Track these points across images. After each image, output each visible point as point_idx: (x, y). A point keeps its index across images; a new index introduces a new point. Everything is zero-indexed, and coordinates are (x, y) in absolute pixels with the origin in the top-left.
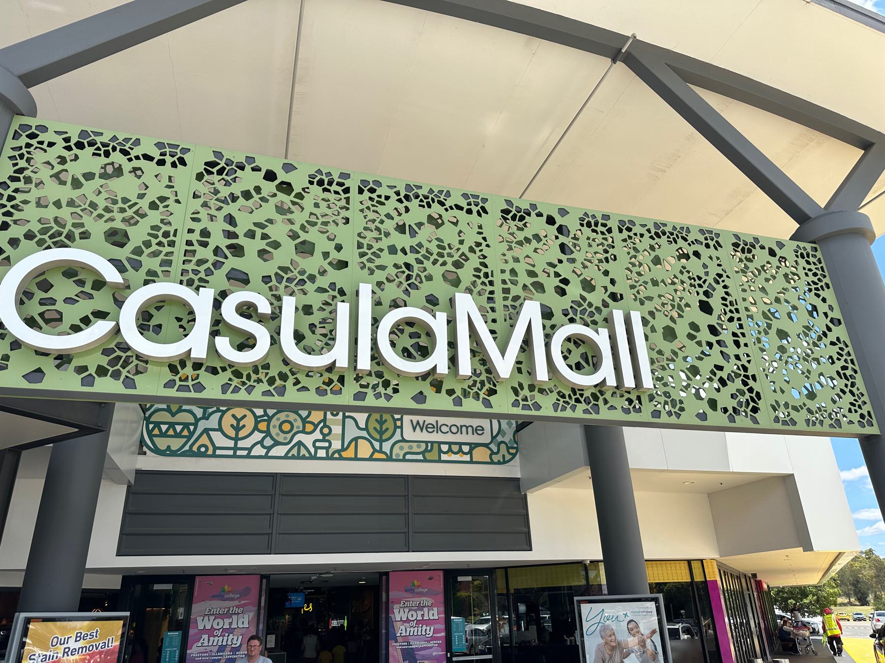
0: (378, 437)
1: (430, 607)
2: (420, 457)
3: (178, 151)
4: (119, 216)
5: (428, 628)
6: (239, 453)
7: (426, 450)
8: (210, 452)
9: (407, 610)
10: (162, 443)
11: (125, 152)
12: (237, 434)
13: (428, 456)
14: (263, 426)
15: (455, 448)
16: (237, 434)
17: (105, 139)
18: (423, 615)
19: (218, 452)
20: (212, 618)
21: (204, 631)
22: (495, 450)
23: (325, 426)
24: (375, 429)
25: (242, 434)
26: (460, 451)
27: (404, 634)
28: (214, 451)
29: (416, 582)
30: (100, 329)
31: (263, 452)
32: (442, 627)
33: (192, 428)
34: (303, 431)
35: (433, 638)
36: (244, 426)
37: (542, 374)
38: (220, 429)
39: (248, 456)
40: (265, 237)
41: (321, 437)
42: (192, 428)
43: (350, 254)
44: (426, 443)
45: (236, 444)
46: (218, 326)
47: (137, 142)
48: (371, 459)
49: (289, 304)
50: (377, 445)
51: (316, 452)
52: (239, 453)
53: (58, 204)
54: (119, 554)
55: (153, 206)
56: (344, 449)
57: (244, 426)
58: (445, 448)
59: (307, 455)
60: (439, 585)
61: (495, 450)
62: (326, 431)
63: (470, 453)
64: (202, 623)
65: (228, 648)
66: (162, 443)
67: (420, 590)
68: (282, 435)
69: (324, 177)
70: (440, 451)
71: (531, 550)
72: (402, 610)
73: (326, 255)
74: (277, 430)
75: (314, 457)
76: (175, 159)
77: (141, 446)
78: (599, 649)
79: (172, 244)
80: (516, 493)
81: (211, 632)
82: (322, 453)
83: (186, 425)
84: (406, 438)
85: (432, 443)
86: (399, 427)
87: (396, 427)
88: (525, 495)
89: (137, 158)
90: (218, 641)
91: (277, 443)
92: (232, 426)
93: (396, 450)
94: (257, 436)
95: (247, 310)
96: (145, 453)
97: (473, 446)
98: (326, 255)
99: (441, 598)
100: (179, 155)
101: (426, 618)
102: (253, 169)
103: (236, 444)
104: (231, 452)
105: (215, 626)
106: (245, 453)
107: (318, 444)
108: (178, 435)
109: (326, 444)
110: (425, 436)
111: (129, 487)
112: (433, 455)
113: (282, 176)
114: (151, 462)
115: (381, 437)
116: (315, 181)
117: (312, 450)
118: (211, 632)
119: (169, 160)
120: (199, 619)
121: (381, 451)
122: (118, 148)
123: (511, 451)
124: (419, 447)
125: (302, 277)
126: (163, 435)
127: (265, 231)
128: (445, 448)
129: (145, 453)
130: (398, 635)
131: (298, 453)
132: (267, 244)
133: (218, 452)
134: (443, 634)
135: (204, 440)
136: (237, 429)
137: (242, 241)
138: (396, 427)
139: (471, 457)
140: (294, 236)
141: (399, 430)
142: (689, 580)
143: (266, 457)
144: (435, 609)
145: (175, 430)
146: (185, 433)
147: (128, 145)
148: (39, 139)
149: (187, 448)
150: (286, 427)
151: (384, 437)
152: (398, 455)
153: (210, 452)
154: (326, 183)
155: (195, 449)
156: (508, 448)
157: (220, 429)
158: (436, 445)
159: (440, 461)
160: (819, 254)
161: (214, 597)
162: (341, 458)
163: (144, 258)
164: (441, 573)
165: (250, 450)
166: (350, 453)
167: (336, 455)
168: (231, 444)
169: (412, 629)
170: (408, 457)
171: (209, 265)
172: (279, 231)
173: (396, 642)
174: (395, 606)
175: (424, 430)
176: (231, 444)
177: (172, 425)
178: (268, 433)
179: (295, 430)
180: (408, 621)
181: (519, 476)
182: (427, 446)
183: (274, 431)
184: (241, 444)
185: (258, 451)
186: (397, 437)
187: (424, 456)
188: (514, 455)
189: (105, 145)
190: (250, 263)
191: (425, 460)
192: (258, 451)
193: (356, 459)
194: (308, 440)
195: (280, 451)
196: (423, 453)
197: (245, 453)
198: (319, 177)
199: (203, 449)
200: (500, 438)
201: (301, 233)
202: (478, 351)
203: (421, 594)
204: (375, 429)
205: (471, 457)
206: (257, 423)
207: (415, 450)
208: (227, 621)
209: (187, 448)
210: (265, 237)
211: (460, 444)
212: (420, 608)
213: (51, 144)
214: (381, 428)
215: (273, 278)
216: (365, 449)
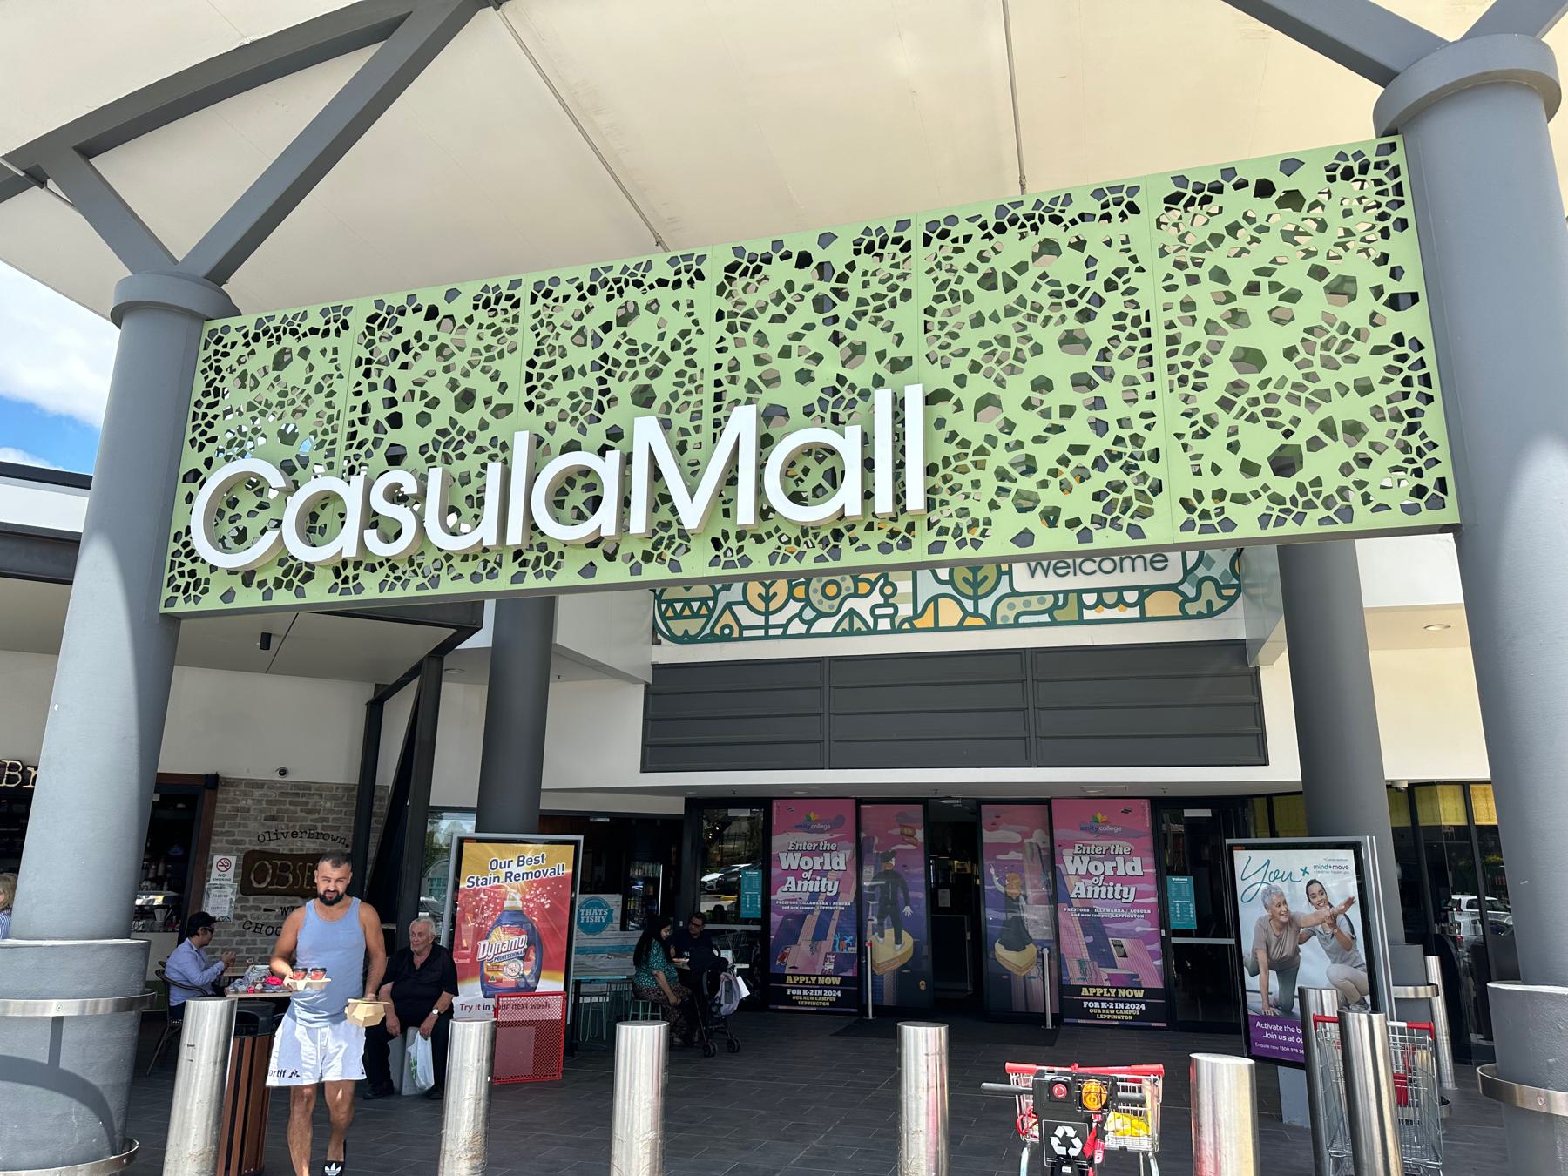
0: (970, 591)
1: (1128, 857)
2: (1045, 618)
3: (1124, 194)
4: (1071, 313)
5: (1126, 889)
6: (772, 632)
7: (1055, 606)
8: (736, 634)
9: (1086, 859)
10: (678, 627)
11: (1056, 220)
12: (767, 607)
13: (1059, 615)
14: (799, 592)
15: (1110, 598)
16: (767, 607)
17: (1027, 209)
18: (822, 864)
19: (746, 633)
20: (798, 855)
21: (790, 871)
22: (1191, 593)
23: (887, 583)
24: (965, 579)
25: (773, 605)
26: (1121, 601)
27: (1083, 895)
28: (741, 633)
29: (1099, 816)
30: (272, 536)
31: (802, 628)
32: (1152, 888)
33: (711, 603)
34: (856, 595)
35: (1134, 905)
36: (775, 594)
37: (745, 513)
38: (745, 602)
39: (784, 636)
40: (1275, 287)
41: (882, 601)
42: (711, 603)
43: (517, 395)
44: (1055, 593)
45: (767, 620)
46: (371, 519)
47: (1068, 199)
48: (960, 627)
49: (435, 477)
50: (969, 605)
51: (876, 624)
52: (772, 632)
53: (995, 318)
54: (643, 770)
55: (1110, 286)
56: (917, 616)
57: (775, 594)
58: (1090, 599)
59: (864, 629)
60: (1143, 819)
61: (1191, 593)
62: (888, 590)
63: (1140, 603)
64: (787, 862)
65: (822, 897)
66: (678, 627)
67: (1109, 828)
68: (827, 603)
69: (1351, 163)
70: (1082, 606)
71: (1266, 763)
72: (1077, 858)
73: (1378, 291)
74: (819, 596)
75: (873, 631)
76: (1123, 207)
77: (654, 634)
78: (1261, 925)
79: (1147, 333)
80: (1237, 668)
81: (798, 873)
82: (884, 624)
83: (704, 601)
84: (1018, 588)
85: (1066, 593)
86: (1005, 573)
87: (1000, 573)
88: (1257, 671)
89: (1073, 222)
90: (808, 885)
91: (821, 615)
92: (760, 595)
93: (1002, 610)
94: (793, 607)
95: (395, 495)
96: (659, 643)
97: (1145, 592)
98: (1378, 291)
99: (1148, 843)
100: (1127, 200)
101: (1121, 872)
102: (1237, 186)
103: (767, 620)
104: (761, 633)
105: (1092, 871)
106: (779, 631)
107: (878, 611)
108: (695, 615)
109: (890, 611)
110: (1054, 583)
111: (647, 686)
112: (1070, 612)
113: (1282, 184)
114: (670, 653)
115: (976, 592)
116: (1338, 173)
117: (870, 621)
118: (798, 873)
119: (1114, 211)
120: (782, 856)
121: (976, 614)
122: (1047, 216)
123: (1225, 592)
124: (1042, 601)
125: (1344, 337)
126: (678, 616)
127: (1273, 278)
128: (1090, 599)
129: (659, 643)
130: (1073, 895)
131: (851, 626)
132: (1281, 298)
133: (746, 633)
134: (1153, 900)
135: (727, 618)
136: (767, 599)
137: (1243, 302)
138: (1000, 573)
139: (1142, 611)
140: (1318, 273)
141: (1005, 578)
142: (1463, 822)
143: (808, 635)
144: (1137, 860)
145: (691, 608)
146: (704, 611)
147: (1058, 207)
148: (952, 236)
149: (707, 631)
150: (832, 590)
151: (981, 591)
152: (1005, 617)
153: (736, 634)
154: (1356, 170)
155: (717, 631)
156: (1219, 588)
157: (745, 602)
158: (1073, 597)
159: (1081, 621)
160: (1397, 158)
161: (798, 828)
162: (914, 630)
163: (1114, 362)
164: (1146, 804)
165: (785, 626)
166: (927, 621)
167: (906, 626)
168: (761, 620)
169: (1097, 889)
170: (1022, 620)
171: (1116, 352)
172: (1293, 274)
173: (1071, 906)
174: (1065, 852)
175: (1051, 572)
176: (761, 620)
177: (687, 602)
178: (807, 602)
179: (844, 593)
180: (1088, 875)
181: (1242, 635)
182: (1056, 599)
183: (816, 598)
184: (773, 620)
185: (797, 627)
186: (1004, 588)
187: (1051, 616)
188: (1231, 600)
189: (1029, 217)
190: (411, 436)
191: (1054, 623)
192: (797, 627)
193: (936, 628)
194: (863, 606)
195: (825, 625)
196: (1049, 611)
197: (779, 631)
198: (1343, 165)
199: (727, 631)
200: (1201, 572)
201: (1329, 265)
202: (660, 499)
203: (1110, 836)
204: (965, 579)
205: (1142, 611)
206: (791, 588)
207: (1036, 606)
208: (818, 860)
209: (707, 631)
210: (1275, 287)
211: (1120, 590)
212: (1110, 856)
213: (967, 239)
214: (975, 577)
215: (1300, 347)
216: (950, 613)
